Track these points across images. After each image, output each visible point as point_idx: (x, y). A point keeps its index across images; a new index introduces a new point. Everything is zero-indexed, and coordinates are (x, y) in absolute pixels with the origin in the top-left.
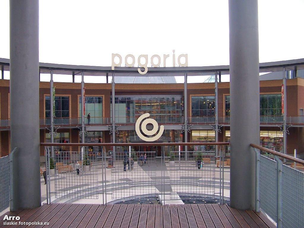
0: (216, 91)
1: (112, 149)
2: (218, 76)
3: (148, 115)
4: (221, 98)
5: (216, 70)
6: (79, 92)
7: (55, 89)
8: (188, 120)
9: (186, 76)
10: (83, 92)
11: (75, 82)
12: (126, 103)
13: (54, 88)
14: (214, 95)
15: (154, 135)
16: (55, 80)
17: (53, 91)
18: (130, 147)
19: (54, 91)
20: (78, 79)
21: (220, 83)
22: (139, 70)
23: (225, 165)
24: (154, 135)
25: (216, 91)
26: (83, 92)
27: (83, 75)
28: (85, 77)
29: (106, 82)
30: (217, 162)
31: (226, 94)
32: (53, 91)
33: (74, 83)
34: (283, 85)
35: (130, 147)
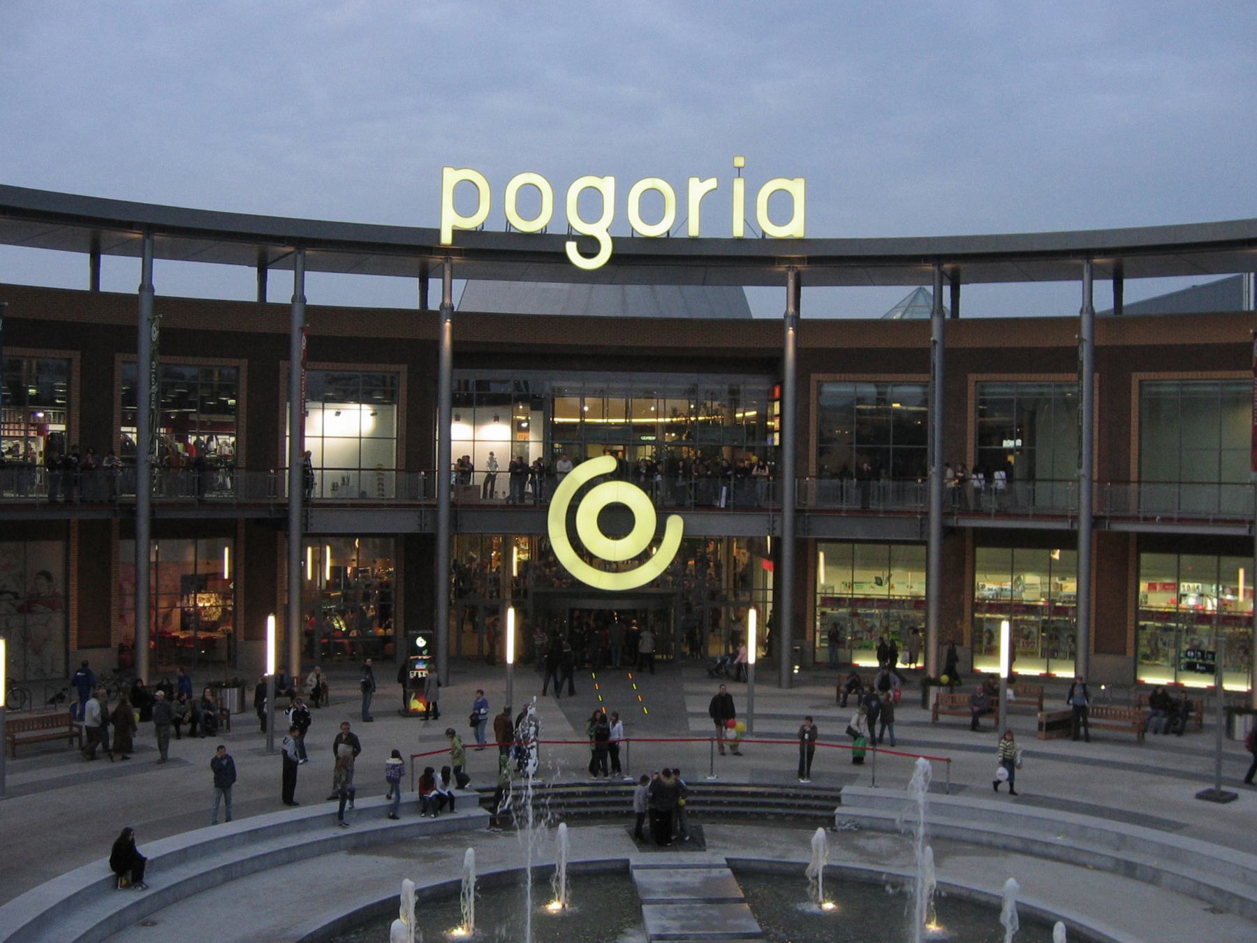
0: (937, 358)
1: (981, 619)
2: (947, 290)
3: (606, 464)
4: (954, 400)
5: (938, 259)
6: (126, 338)
7: (161, 330)
8: (800, 492)
9: (937, 284)
10: (299, 344)
11: (103, 288)
12: (821, 408)
13: (157, 323)
14: (923, 377)
15: (644, 557)
16: (968, 310)
17: (149, 334)
18: (977, 615)
19: (155, 336)
20: (281, 287)
21: (954, 324)
22: (571, 249)
23: (944, 713)
24: (644, 557)
25: (937, 358)
26: (299, 344)
27: (148, 251)
28: (309, 276)
29: (254, 298)
30: (932, 700)
31: (984, 377)
32: (149, 334)
33: (262, 307)
34: (1081, 340)
35: (977, 615)
